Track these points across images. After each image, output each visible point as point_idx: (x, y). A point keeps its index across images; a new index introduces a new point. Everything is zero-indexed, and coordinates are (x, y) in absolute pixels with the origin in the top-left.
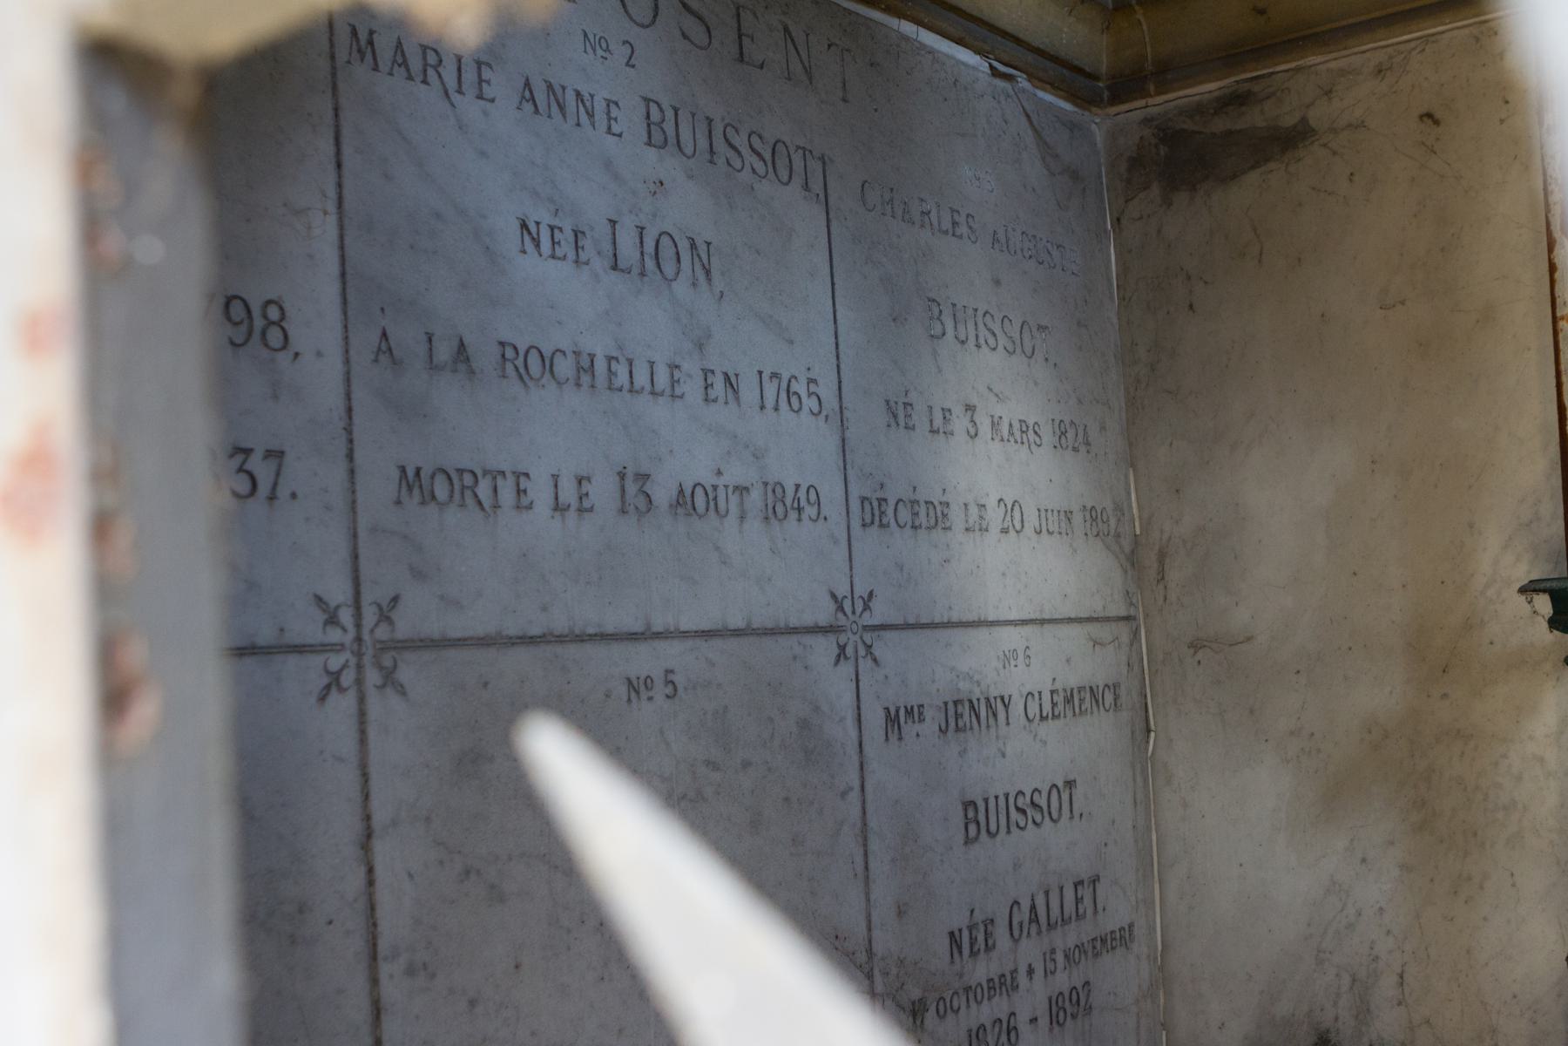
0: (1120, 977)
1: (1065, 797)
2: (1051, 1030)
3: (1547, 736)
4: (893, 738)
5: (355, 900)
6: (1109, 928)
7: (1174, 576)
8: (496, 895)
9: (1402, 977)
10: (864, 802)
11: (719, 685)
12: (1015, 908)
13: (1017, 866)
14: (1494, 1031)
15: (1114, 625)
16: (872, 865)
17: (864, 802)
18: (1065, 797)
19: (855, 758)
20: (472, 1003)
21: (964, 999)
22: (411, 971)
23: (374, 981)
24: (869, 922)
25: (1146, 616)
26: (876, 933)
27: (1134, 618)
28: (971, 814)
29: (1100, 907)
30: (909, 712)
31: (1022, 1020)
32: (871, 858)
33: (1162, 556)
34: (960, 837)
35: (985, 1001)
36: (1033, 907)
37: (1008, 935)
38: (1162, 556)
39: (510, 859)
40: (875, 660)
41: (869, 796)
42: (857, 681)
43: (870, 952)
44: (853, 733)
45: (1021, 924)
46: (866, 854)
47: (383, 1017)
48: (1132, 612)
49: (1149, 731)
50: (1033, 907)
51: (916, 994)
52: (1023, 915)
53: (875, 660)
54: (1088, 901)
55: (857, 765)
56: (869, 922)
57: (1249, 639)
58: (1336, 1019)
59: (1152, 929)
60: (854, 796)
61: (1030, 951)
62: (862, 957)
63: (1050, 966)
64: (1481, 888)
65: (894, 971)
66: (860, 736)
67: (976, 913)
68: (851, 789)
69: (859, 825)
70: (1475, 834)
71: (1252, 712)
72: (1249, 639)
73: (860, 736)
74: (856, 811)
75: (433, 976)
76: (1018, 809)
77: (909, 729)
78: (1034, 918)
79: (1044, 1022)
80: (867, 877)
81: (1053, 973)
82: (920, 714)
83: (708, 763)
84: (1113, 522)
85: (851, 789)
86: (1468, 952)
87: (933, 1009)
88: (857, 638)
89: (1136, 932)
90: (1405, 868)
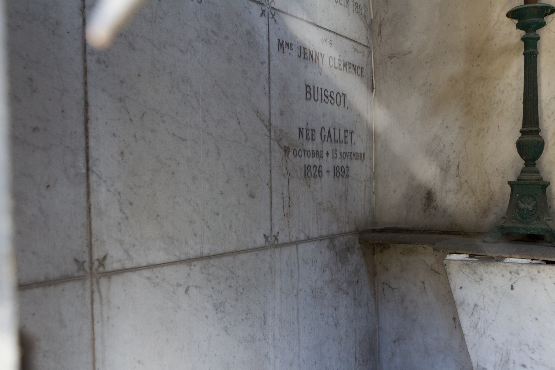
0: (358, 169)
1: (342, 99)
2: (334, 178)
3: (513, 76)
4: (281, 51)
5: (78, 28)
6: (356, 151)
7: (385, 32)
8: (132, 47)
9: (458, 167)
10: (269, 69)
11: (217, 6)
12: (323, 129)
13: (324, 115)
14: (489, 182)
15: (362, 47)
16: (271, 92)
17: (269, 69)
18: (342, 99)
19: (267, 52)
20: (122, 82)
21: (303, 153)
22: (99, 61)
23: (85, 61)
24: (270, 112)
25: (374, 48)
26: (272, 117)
27: (370, 48)
28: (308, 90)
29: (353, 142)
30: (287, 44)
31: (324, 169)
32: (271, 90)
33: (380, 26)
34: (304, 96)
35: (311, 158)
36: (329, 132)
37: (320, 137)
38: (380, 26)
39: (137, 36)
40: (275, 21)
41: (271, 68)
42: (269, 25)
43: (270, 122)
44: (267, 43)
45: (325, 136)
46: (269, 88)
47: (88, 74)
48: (369, 45)
49: (373, 89)
50: (329, 132)
51: (286, 144)
52: (325, 133)
53: (275, 21)
54: (349, 138)
55: (267, 55)
56: (270, 112)
57: (410, 52)
58: (435, 184)
59: (371, 158)
60: (266, 65)
61: (327, 147)
62: (267, 124)
63: (335, 155)
64: (487, 132)
65: (278, 133)
66: (269, 45)
67: (309, 125)
68: (265, 62)
69: (267, 76)
70: (486, 113)
71: (410, 78)
72: (410, 52)
73: (269, 45)
74: (266, 71)
75: (107, 67)
76: (325, 95)
77: (287, 50)
78: (329, 136)
79: (332, 173)
80: (270, 96)
81: (336, 158)
82: (291, 47)
83: (212, 31)
84: (363, 10)
85: (265, 62)
86: (482, 155)
87: (292, 152)
88: (269, 10)
89: (366, 157)
90: (461, 128)
